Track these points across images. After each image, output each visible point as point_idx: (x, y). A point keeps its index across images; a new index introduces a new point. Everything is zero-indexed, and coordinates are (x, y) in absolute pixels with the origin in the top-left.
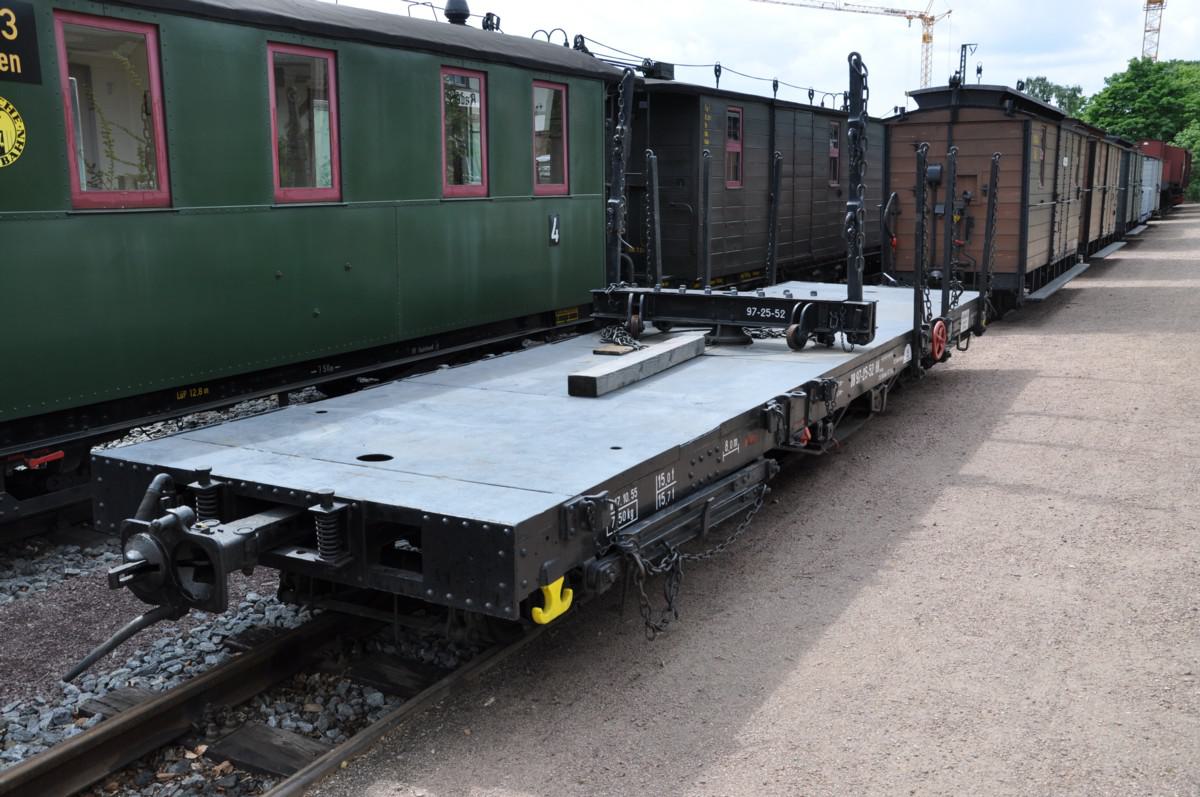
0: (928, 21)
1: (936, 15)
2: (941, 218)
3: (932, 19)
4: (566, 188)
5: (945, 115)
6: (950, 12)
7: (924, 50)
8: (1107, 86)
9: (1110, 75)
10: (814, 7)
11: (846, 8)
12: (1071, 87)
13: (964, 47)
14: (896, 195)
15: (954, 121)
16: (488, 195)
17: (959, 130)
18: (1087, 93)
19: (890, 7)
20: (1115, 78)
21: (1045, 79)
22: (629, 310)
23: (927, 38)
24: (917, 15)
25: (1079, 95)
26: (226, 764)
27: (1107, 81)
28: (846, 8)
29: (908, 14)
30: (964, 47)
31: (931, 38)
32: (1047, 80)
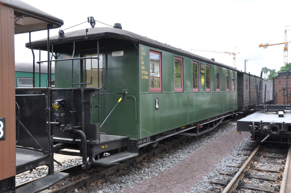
0: (234, 54)
1: (236, 53)
2: (286, 96)
3: (235, 54)
4: (210, 90)
5: (286, 77)
6: (239, 52)
7: (234, 61)
8: (281, 69)
9: (281, 67)
10: (222, 53)
11: (215, 52)
12: (273, 69)
13: (245, 60)
14: (276, 92)
15: (288, 78)
16: (199, 91)
17: (288, 79)
18: (276, 71)
19: (225, 52)
20: (283, 67)
21: (266, 68)
22: (265, 108)
23: (234, 58)
24: (232, 53)
25: (275, 71)
26: (267, 158)
27: (281, 68)
28: (215, 52)
29: (229, 53)
30: (245, 60)
31: (235, 58)
32: (267, 68)
